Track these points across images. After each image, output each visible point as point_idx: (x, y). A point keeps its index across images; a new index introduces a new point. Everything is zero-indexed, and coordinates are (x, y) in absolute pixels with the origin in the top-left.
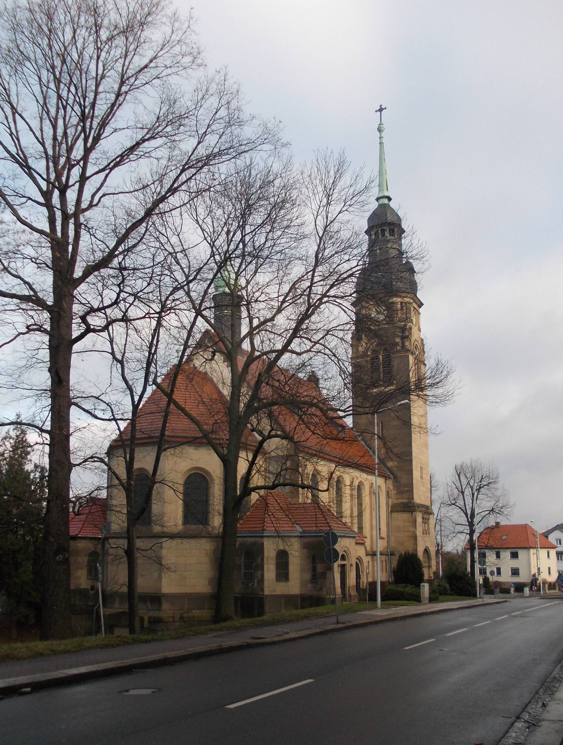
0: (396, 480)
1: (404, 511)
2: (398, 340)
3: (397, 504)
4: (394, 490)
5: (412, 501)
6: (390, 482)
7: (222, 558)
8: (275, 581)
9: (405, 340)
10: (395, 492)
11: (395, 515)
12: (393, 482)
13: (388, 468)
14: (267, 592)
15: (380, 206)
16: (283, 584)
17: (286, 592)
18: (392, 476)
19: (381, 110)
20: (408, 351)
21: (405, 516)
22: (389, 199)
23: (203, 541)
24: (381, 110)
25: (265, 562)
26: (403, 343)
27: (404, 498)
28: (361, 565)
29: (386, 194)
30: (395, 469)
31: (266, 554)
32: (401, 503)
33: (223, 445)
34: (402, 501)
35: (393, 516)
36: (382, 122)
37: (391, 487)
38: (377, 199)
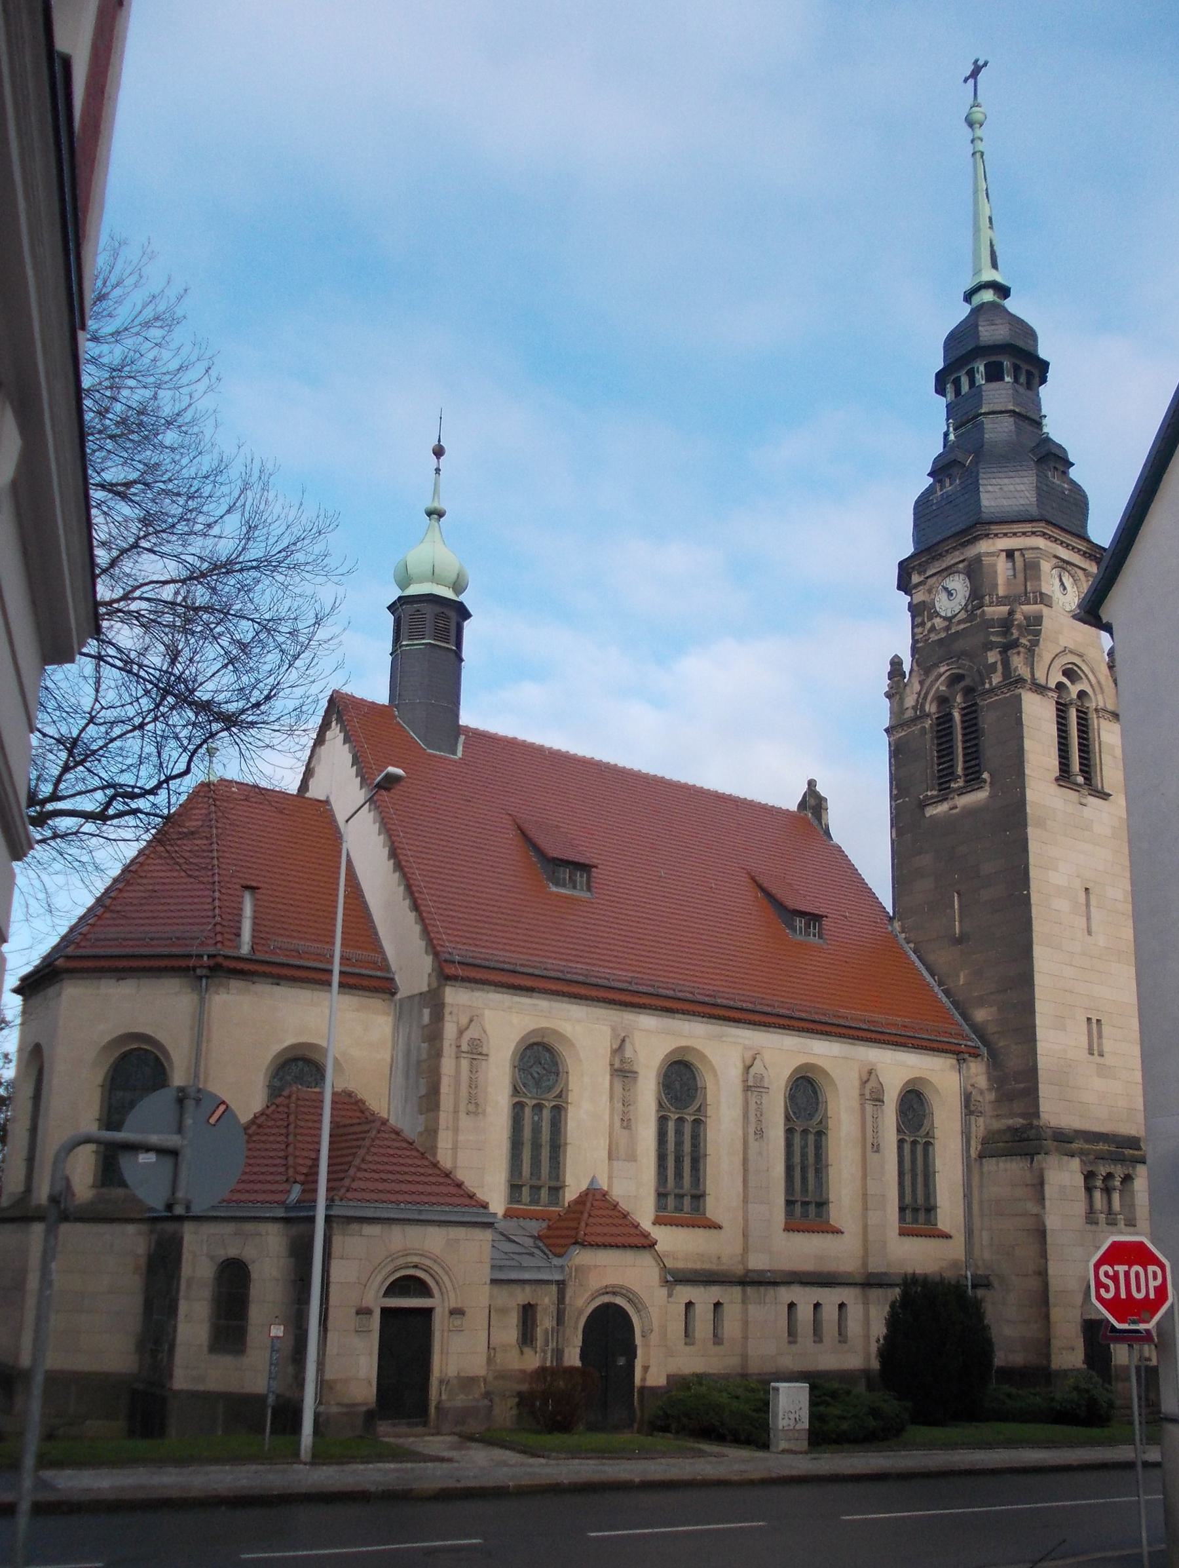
0: (995, 1060)
1: (1009, 1154)
2: (993, 657)
3: (999, 1132)
4: (990, 1090)
5: (1035, 1122)
6: (977, 1071)
7: (706, 1282)
8: (205, 1349)
9: (1009, 653)
10: (991, 1096)
11: (990, 1165)
12: (988, 1066)
13: (975, 1028)
14: (181, 1381)
15: (977, 311)
16: (227, 1360)
17: (233, 1386)
18: (984, 1051)
19: (975, 73)
20: (1020, 681)
21: (1011, 1169)
22: (1003, 291)
23: (131, 1229)
24: (975, 73)
25: (182, 1294)
26: (1006, 664)
27: (1012, 1115)
28: (638, 1311)
29: (989, 275)
30: (991, 1029)
31: (186, 1270)
32: (1009, 1128)
33: (199, 972)
34: (1010, 1122)
35: (985, 1169)
36: (980, 100)
37: (982, 1081)
38: (968, 297)
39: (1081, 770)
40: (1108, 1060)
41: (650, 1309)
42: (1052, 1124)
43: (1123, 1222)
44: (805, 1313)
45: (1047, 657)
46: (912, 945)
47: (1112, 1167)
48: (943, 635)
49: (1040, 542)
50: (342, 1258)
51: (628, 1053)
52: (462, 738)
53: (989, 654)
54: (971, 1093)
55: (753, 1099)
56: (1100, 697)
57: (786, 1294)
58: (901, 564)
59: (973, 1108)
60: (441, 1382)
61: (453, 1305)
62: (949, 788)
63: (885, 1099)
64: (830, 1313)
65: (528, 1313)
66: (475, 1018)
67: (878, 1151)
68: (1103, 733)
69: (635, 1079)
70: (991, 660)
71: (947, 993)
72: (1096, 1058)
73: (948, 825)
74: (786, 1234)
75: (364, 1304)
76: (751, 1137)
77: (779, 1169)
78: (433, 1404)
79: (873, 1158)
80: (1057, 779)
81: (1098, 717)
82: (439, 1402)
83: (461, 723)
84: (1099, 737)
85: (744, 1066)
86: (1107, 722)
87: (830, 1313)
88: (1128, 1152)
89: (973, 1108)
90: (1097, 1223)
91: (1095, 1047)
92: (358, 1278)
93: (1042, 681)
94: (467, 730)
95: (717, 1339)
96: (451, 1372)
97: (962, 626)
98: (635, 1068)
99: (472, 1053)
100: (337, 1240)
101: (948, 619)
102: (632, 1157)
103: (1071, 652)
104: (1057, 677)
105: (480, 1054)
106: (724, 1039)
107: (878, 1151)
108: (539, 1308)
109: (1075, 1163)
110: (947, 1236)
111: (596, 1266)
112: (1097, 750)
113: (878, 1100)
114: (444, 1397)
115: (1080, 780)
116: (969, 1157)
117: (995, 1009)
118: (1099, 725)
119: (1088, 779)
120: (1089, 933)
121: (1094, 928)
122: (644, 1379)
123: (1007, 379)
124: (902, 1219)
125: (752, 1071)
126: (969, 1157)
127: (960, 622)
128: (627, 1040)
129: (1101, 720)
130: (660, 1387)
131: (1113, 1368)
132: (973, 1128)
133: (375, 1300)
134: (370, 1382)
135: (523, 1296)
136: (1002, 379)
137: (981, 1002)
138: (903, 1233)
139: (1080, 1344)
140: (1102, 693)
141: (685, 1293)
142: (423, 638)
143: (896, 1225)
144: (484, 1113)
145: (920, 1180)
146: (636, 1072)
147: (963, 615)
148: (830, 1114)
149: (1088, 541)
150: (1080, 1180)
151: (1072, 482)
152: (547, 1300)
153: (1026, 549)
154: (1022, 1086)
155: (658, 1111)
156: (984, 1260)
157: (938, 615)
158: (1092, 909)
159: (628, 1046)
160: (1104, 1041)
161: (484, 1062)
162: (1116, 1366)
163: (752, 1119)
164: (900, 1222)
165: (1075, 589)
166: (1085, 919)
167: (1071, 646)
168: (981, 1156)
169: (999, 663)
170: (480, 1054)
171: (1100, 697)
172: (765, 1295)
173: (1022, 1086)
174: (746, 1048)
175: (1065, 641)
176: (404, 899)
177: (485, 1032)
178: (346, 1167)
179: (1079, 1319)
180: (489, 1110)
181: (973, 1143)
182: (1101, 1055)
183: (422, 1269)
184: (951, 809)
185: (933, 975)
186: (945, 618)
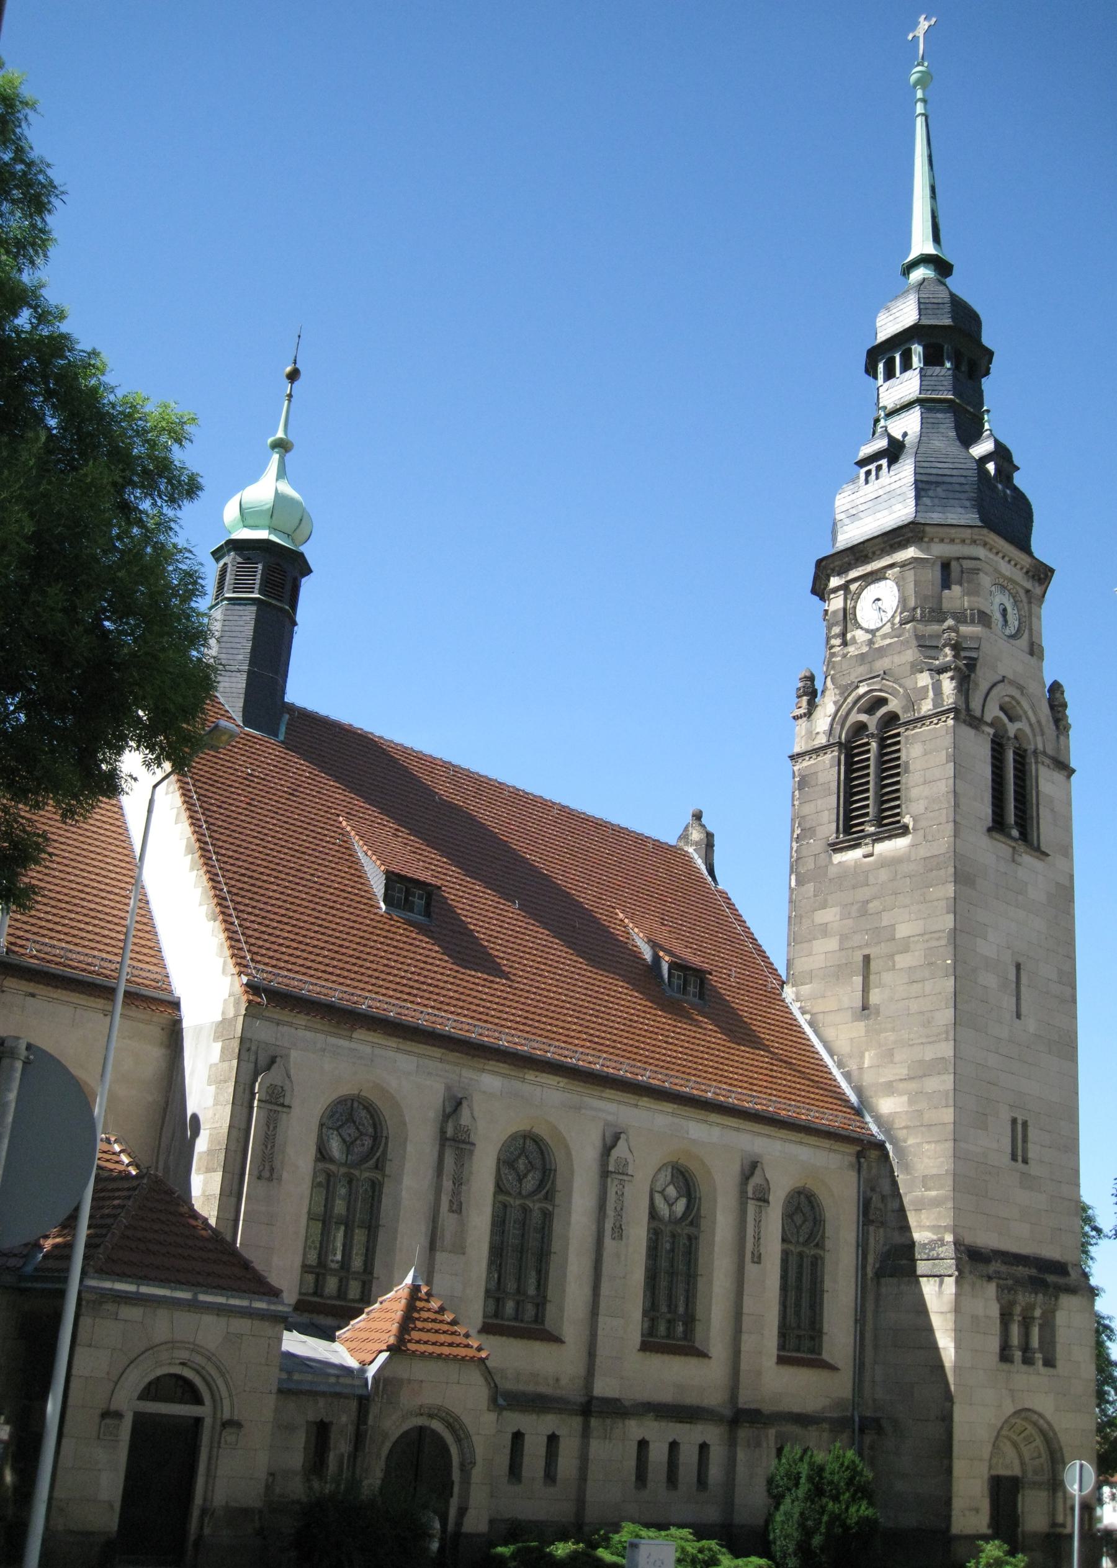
30: (899, 1123)
35: (883, 1290)
39: (1016, 823)
40: (1034, 1169)
41: (474, 1438)
42: (966, 1242)
43: (1040, 1362)
44: (658, 1453)
45: (984, 686)
46: (808, 1017)
47: (1033, 1296)
48: (865, 649)
49: (981, 552)
50: (90, 1346)
51: (465, 1119)
52: (287, 716)
53: (919, 676)
54: (871, 1198)
55: (612, 1189)
56: (1039, 739)
57: (635, 1429)
58: (819, 563)
59: (872, 1217)
60: (204, 1511)
61: (227, 1416)
62: (862, 831)
63: (771, 1199)
64: (688, 1456)
65: (321, 1432)
66: (278, 1059)
67: (759, 1262)
68: (1041, 781)
69: (471, 1152)
70: (921, 684)
71: (848, 1076)
72: (1020, 1165)
73: (857, 877)
74: (641, 1354)
75: (113, 1407)
76: (608, 1232)
77: (638, 1276)
78: (198, 1500)
79: (750, 1268)
80: (990, 830)
81: (1037, 763)
82: (200, 1537)
83: (286, 700)
84: (1037, 787)
85: (604, 1145)
86: (1046, 769)
87: (688, 1456)
88: (1051, 1278)
89: (872, 1217)
90: (1012, 1362)
91: (1020, 1152)
92: (108, 1373)
93: (978, 713)
94: (291, 709)
95: (550, 1476)
96: (219, 1498)
97: (888, 641)
98: (473, 1139)
99: (271, 1103)
100: (86, 1321)
101: (873, 632)
102: (459, 1249)
103: (1012, 683)
104: (993, 712)
105: (283, 1105)
106: (583, 1111)
107: (759, 1262)
108: (334, 1428)
109: (991, 1289)
110: (832, 1368)
111: (409, 1381)
112: (1034, 801)
113: (763, 1199)
114: (207, 1531)
115: (1015, 833)
116: (864, 1275)
117: (905, 1098)
118: (1037, 770)
119: (1025, 837)
120: (1019, 1016)
121: (1024, 1010)
122: (459, 1524)
123: (948, 365)
124: (782, 1347)
125: (615, 1153)
126: (864, 1275)
127: (884, 637)
128: (465, 1104)
129: (1041, 767)
130: (479, 1535)
131: (1020, 1536)
132: (872, 1241)
133: (127, 1400)
134: (111, 1506)
135: (316, 1411)
136: (942, 364)
137: (890, 1088)
138: (781, 1361)
139: (985, 1505)
140: (1042, 735)
141: (518, 1420)
142: (252, 592)
143: (775, 1352)
144: (280, 1179)
145: (805, 1296)
146: (473, 1144)
147: (887, 629)
148: (703, 1212)
149: (1034, 557)
150: (995, 1310)
151: (1015, 489)
152: (344, 1419)
153: (964, 558)
154: (933, 1193)
155: (495, 1194)
156: (874, 1400)
157: (860, 627)
158: (1023, 989)
159: (465, 1111)
160: (1030, 1146)
161: (284, 1116)
162: (1023, 1532)
163: (610, 1212)
164: (779, 1350)
165: (1016, 612)
166: (1015, 999)
167: (1010, 676)
168: (879, 1275)
169: (930, 687)
170: (283, 1105)
171: (1039, 739)
172: (611, 1429)
173: (933, 1193)
174: (607, 1124)
175: (1004, 669)
176: (200, 905)
177: (289, 1077)
178: (104, 1231)
179: (986, 1477)
180: (285, 1175)
181: (871, 1259)
182: (1025, 1161)
183: (190, 1367)
184: (865, 856)
185: (832, 1056)
186: (867, 631)
